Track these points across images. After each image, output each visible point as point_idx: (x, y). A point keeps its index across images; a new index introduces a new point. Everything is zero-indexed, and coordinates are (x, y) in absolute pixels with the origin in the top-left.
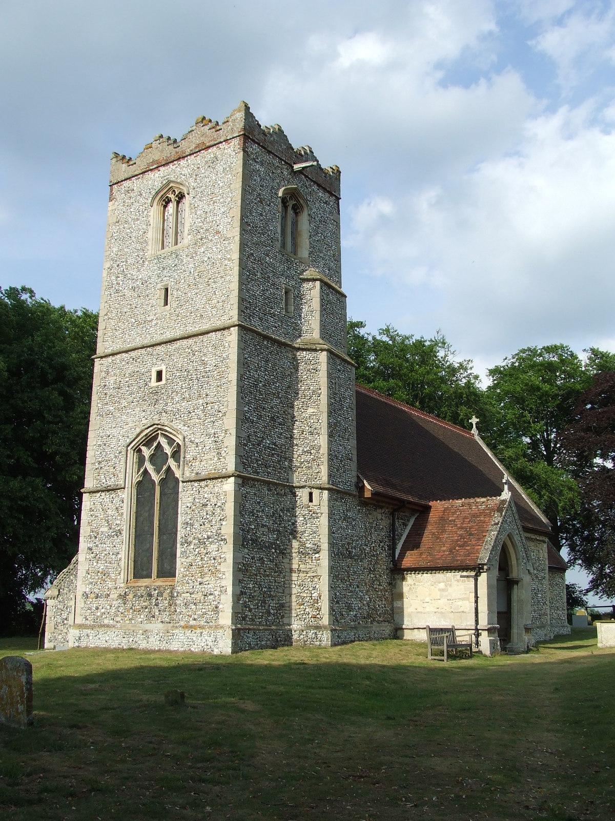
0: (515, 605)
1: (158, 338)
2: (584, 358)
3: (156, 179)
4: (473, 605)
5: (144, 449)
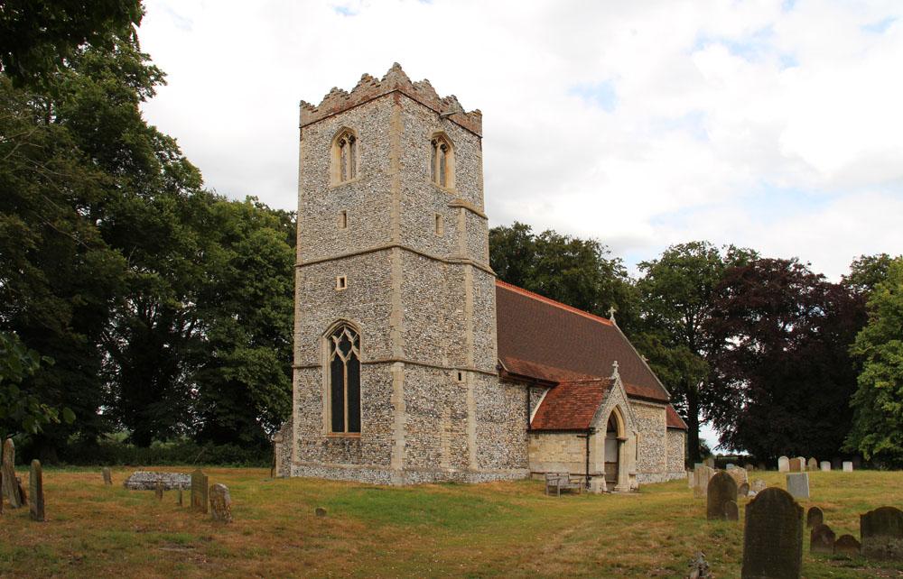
0: (622, 457)
1: (340, 254)
2: (723, 254)
3: (333, 125)
4: (586, 457)
5: (334, 337)
